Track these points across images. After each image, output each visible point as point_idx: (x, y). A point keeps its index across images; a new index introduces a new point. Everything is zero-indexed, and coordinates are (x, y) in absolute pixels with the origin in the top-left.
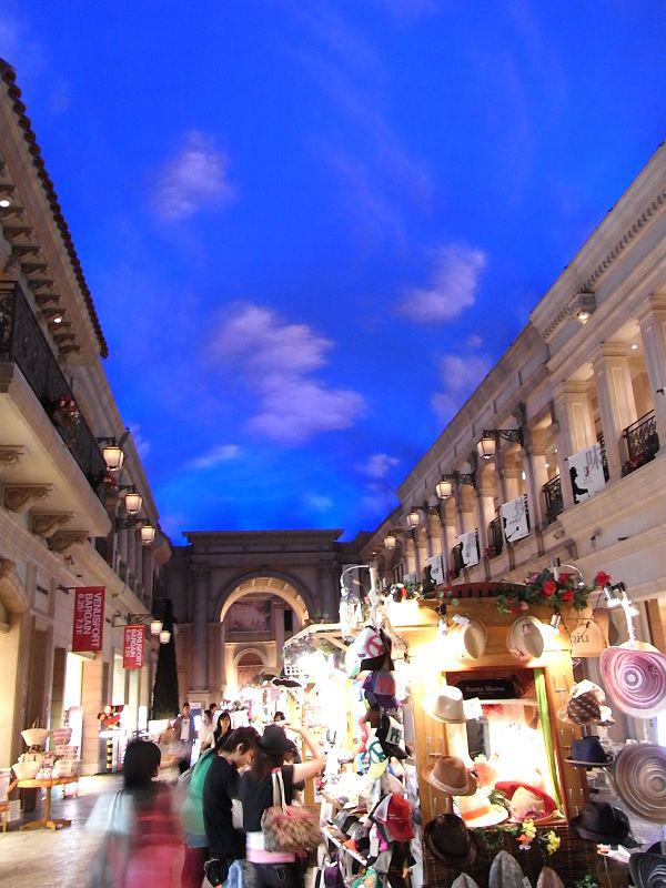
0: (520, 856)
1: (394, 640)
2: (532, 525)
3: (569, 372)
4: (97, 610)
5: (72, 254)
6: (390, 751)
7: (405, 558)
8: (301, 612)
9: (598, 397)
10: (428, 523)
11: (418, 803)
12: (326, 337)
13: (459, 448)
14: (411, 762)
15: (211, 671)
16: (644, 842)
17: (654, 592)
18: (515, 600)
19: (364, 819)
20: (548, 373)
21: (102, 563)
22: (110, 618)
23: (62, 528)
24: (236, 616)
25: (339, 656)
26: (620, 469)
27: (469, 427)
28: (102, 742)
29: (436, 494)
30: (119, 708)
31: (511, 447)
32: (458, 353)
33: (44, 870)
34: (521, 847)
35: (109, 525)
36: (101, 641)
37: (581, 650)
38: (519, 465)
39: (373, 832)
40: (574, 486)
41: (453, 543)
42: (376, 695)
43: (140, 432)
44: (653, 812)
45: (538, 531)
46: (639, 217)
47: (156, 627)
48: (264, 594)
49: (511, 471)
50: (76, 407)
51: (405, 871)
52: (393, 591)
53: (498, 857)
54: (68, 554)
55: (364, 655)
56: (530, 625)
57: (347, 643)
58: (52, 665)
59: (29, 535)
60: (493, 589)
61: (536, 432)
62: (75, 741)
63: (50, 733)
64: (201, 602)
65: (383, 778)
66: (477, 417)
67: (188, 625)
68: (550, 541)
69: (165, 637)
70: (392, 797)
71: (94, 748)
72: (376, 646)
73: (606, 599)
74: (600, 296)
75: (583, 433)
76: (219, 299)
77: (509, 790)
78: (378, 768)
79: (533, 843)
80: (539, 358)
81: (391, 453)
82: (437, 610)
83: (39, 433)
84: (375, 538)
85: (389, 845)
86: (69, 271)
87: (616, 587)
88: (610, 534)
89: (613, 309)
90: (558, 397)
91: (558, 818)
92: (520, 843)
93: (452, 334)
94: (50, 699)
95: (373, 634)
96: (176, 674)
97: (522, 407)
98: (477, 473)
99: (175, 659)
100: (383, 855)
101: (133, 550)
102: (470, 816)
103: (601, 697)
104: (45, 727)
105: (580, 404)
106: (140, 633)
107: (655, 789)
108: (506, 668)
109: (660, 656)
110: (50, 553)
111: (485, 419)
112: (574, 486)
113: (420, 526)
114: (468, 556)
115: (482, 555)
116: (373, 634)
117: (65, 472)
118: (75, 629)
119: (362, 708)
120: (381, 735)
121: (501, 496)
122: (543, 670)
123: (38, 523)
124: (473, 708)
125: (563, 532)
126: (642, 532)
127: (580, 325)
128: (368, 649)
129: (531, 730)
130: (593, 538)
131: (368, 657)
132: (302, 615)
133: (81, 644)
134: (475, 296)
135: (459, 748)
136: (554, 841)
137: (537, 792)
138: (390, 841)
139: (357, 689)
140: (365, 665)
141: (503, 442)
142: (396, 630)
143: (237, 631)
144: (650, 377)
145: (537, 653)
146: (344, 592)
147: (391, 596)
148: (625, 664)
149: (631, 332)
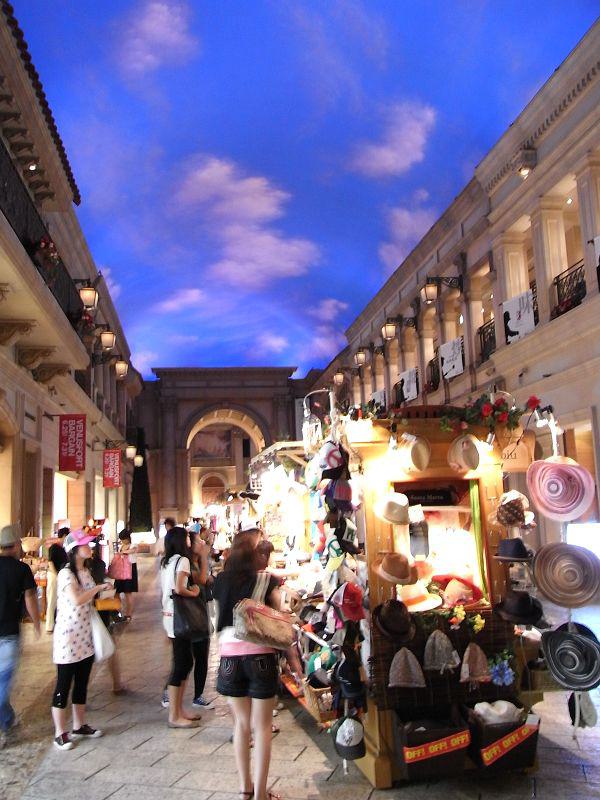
0: (451, 635)
1: (351, 455)
2: (467, 363)
3: (510, 223)
4: (79, 435)
5: (44, 104)
6: (346, 548)
7: (352, 393)
8: (258, 440)
9: (534, 250)
10: (373, 362)
11: (367, 592)
12: (285, 189)
13: (404, 294)
14: (361, 559)
15: (179, 488)
16: (554, 623)
17: (569, 423)
19: (321, 606)
20: (489, 224)
21: (82, 394)
23: (46, 361)
24: (200, 443)
25: (299, 472)
26: (549, 313)
27: (414, 274)
29: (381, 336)
30: (101, 522)
31: (451, 293)
32: (408, 207)
33: (45, 653)
34: (452, 628)
35: (87, 360)
37: (513, 465)
38: (458, 310)
39: (330, 614)
40: (507, 328)
41: (395, 380)
42: (335, 501)
43: (111, 276)
44: (564, 598)
45: (472, 369)
46: (584, 76)
47: (131, 451)
48: (225, 425)
49: (450, 315)
50: (55, 249)
51: (357, 646)
52: (351, 411)
53: (433, 634)
54: (51, 385)
55: (325, 466)
56: (469, 442)
57: (307, 461)
58: (42, 497)
59: (16, 367)
60: (438, 411)
61: (476, 278)
63: (43, 542)
64: (170, 430)
65: (339, 570)
66: (421, 265)
67: (158, 451)
68: (482, 378)
69: (139, 461)
70: (347, 587)
72: (335, 458)
73: (536, 420)
74: (541, 152)
75: (517, 281)
76: (181, 152)
77: (443, 582)
78: (335, 562)
79: (463, 624)
80: (480, 213)
81: (341, 300)
82: (388, 428)
83: (22, 271)
84: (324, 375)
85: (344, 624)
86: (41, 120)
87: (545, 409)
88: (537, 372)
89: (553, 166)
90: (497, 247)
91: (483, 605)
92: (452, 624)
93: (401, 188)
94: (41, 512)
95: (333, 447)
96: (149, 494)
97: (463, 257)
98: (420, 317)
99: (147, 478)
100: (339, 632)
101: (108, 383)
102: (413, 602)
103: (525, 504)
104: (38, 536)
105: (517, 253)
106: (117, 457)
107: (567, 580)
108: (445, 480)
109: (579, 468)
110: (36, 384)
111: (429, 267)
112: (507, 328)
113: (366, 365)
114: (408, 391)
115: (421, 390)
116: (333, 447)
117: (47, 309)
118: (60, 451)
119: (323, 513)
120: (339, 534)
121: (440, 340)
122: (477, 481)
123: (24, 355)
124: (416, 513)
125: (494, 370)
126: (564, 370)
127: (521, 180)
128: (329, 462)
129: (465, 531)
130: (521, 375)
131: (328, 468)
132: (258, 442)
133: (68, 464)
134: (424, 152)
136: (479, 622)
137: (467, 583)
139: (320, 496)
140: (325, 475)
141: (444, 288)
142: (352, 446)
143: (201, 457)
144: (582, 229)
145: (474, 465)
146: (306, 413)
147: (349, 416)
148: (549, 476)
149: (568, 187)
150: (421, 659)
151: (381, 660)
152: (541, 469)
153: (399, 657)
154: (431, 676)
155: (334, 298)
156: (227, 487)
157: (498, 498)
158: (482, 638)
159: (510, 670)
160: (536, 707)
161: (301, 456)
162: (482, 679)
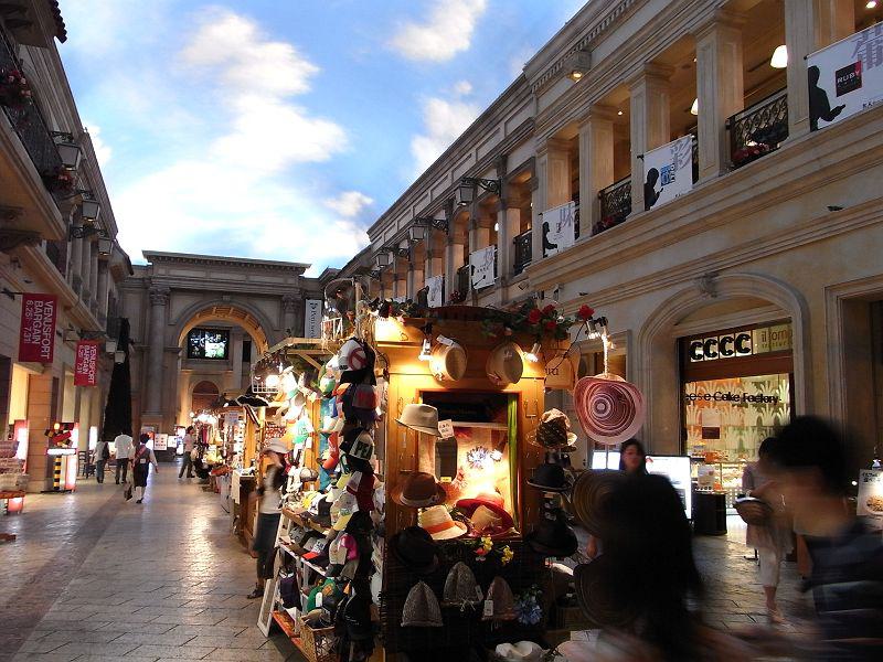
0: (475, 567)
2: (500, 274)
12: (315, 60)
18: (500, 325)
22: (61, 331)
25: (311, 377)
28: (51, 459)
30: (70, 426)
36: (51, 352)
37: (554, 381)
40: (545, 239)
54: (14, 256)
55: (346, 367)
62: (22, 453)
71: (41, 463)
72: (358, 358)
82: (422, 329)
92: (477, 555)
93: (441, 77)
100: (350, 566)
112: (545, 239)
118: (22, 337)
122: (517, 396)
124: (446, 428)
131: (349, 369)
133: (29, 354)
134: (471, 41)
135: (428, 465)
137: (496, 509)
138: (550, 462)
145: (516, 378)
148: (598, 394)
150: (439, 594)
151: (393, 593)
152: (588, 389)
153: (413, 592)
154: (449, 613)
155: (358, 191)
156: (221, 392)
157: (538, 416)
158: (509, 572)
159: (538, 607)
160: (560, 648)
161: (315, 357)
162: (506, 617)
